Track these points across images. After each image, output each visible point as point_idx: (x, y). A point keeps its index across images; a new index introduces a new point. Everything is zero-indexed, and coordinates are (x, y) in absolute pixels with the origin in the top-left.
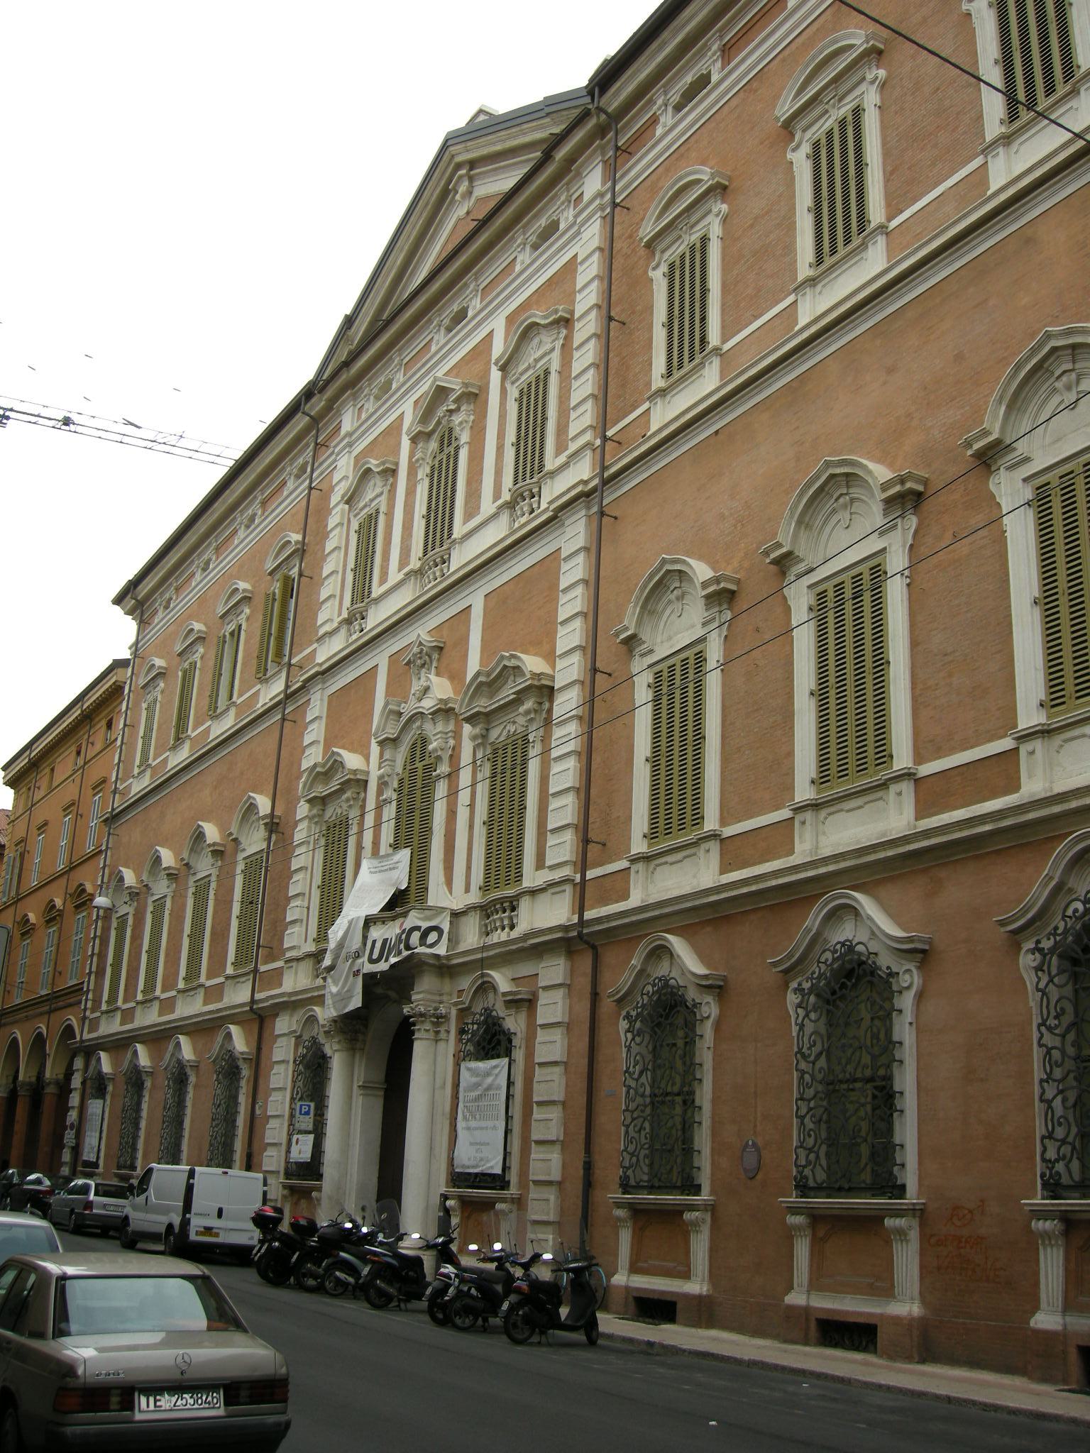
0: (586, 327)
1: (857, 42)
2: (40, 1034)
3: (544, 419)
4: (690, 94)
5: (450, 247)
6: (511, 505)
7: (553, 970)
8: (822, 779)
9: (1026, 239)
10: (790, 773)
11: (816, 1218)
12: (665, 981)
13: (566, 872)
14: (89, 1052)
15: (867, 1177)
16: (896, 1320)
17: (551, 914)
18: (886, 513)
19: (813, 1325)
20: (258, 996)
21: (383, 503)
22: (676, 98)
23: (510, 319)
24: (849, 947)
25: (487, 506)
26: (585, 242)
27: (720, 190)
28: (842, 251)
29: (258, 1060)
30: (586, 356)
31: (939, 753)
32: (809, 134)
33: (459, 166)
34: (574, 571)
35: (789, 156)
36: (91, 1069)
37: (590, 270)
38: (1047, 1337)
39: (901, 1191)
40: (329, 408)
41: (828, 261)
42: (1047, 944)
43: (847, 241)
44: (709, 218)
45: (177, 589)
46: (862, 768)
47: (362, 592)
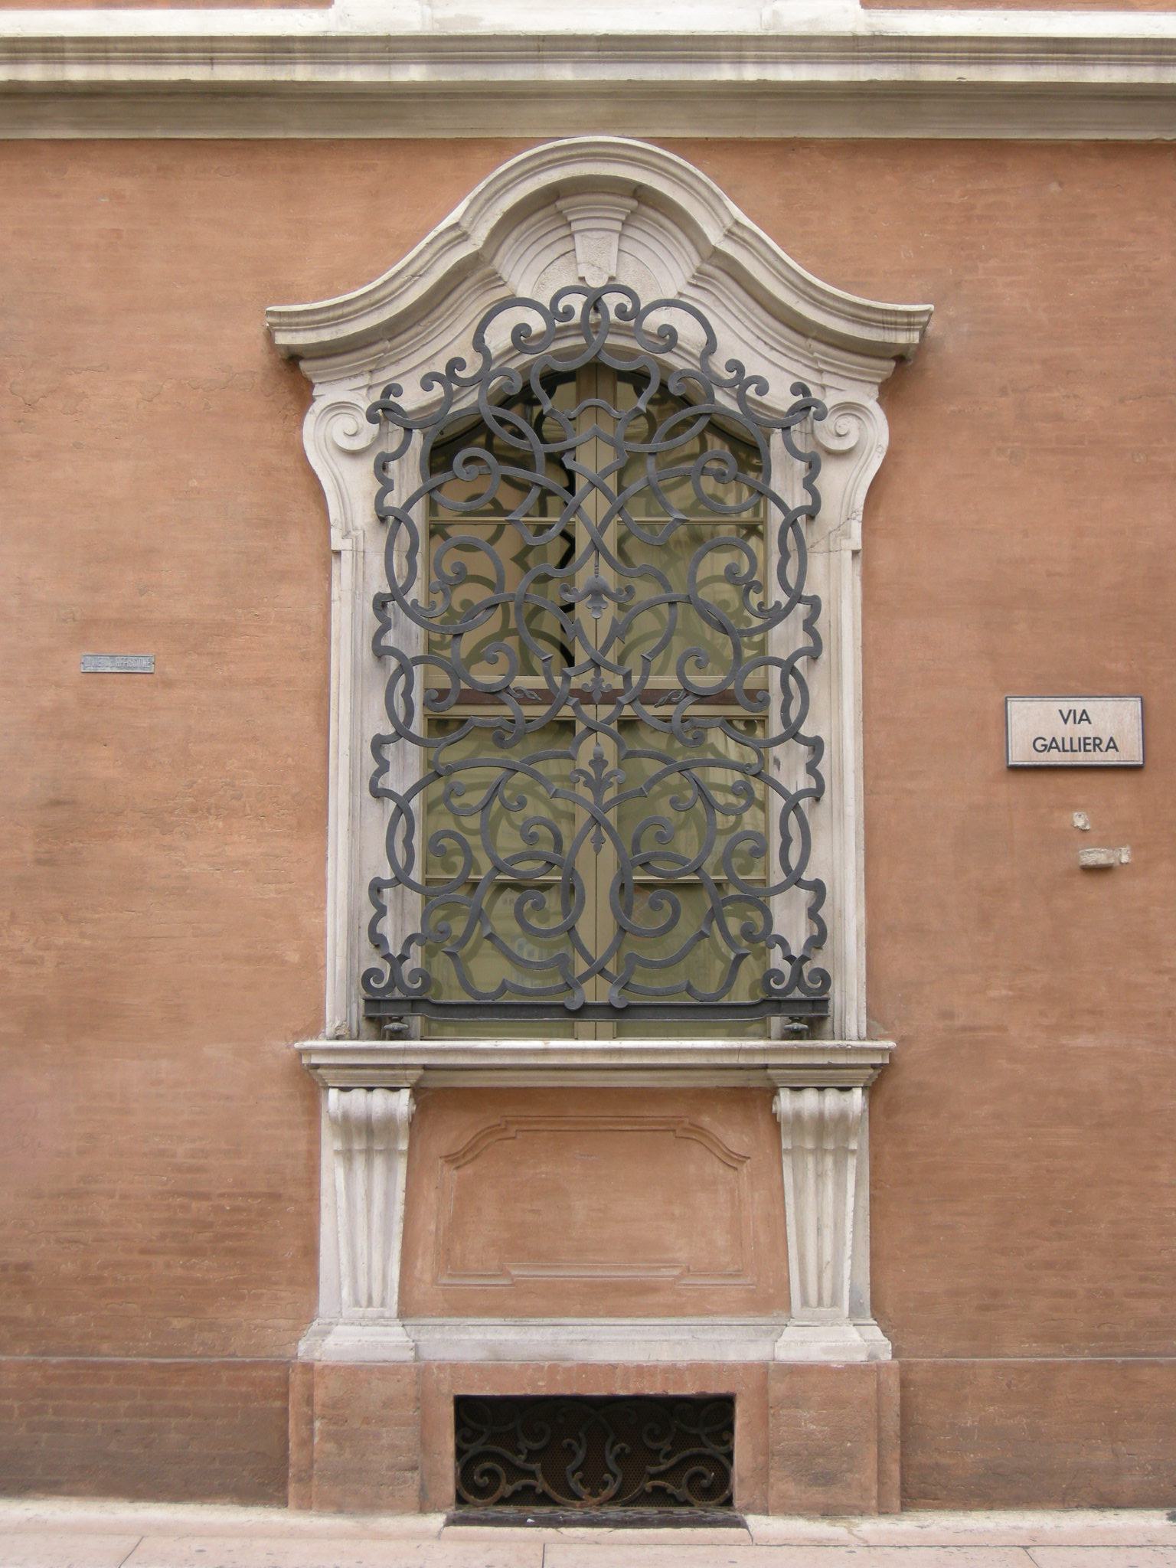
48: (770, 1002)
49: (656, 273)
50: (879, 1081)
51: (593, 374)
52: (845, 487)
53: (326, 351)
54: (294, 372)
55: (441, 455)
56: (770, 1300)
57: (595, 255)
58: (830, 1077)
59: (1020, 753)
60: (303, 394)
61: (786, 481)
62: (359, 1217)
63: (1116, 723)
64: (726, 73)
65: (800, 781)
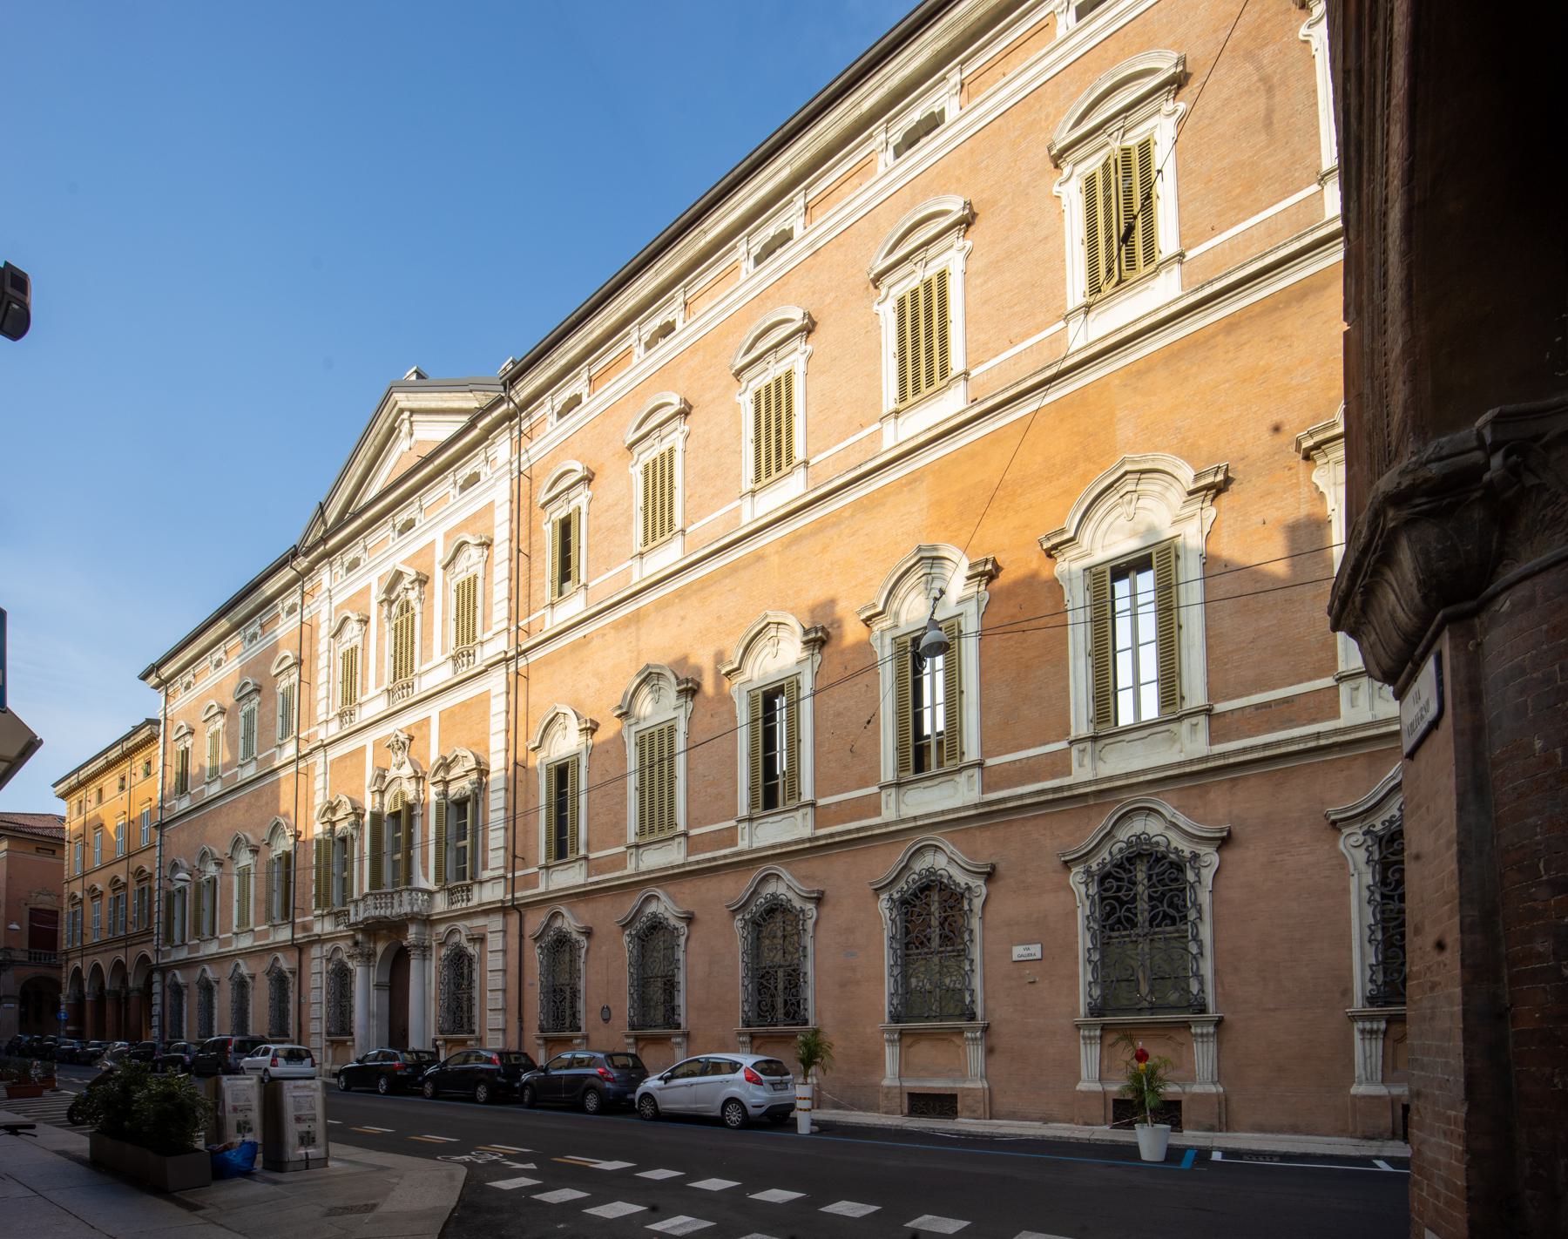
0: (501, 551)
1: (1165, 66)
2: (119, 962)
3: (475, 607)
4: (911, 140)
5: (394, 477)
6: (455, 658)
7: (496, 922)
8: (641, 833)
9: (759, 557)
10: (625, 828)
11: (547, 1040)
12: (560, 929)
13: (501, 872)
14: (164, 970)
15: (660, 1021)
16: (1196, 1097)
17: (492, 893)
18: (678, 698)
19: (906, 1097)
20: (517, 895)
21: (358, 641)
22: (756, 250)
23: (447, 536)
24: (655, 915)
25: (438, 657)
26: (496, 492)
27: (588, 479)
28: (775, 475)
29: (298, 972)
30: (501, 571)
31: (700, 825)
32: (1080, 169)
33: (402, 411)
34: (498, 705)
35: (631, 470)
36: (168, 981)
37: (502, 514)
38: (1088, 1095)
39: (579, 1029)
40: (310, 569)
41: (764, 481)
42: (896, 896)
43: (662, 534)
44: (676, 434)
45: (262, 626)
46: (661, 829)
47: (349, 698)
48: (961, 1016)
49: (1151, 827)
50: (1219, 1023)
51: (1139, 855)
52: (1207, 875)
53: (1341, 820)
54: (1067, 865)
55: (1102, 881)
56: (964, 1077)
57: (1138, 826)
58: (974, 1030)
59: (1015, 958)
60: (1069, 869)
61: (1191, 876)
62: (891, 1056)
63: (1036, 950)
64: (1142, 779)
65: (967, 968)
